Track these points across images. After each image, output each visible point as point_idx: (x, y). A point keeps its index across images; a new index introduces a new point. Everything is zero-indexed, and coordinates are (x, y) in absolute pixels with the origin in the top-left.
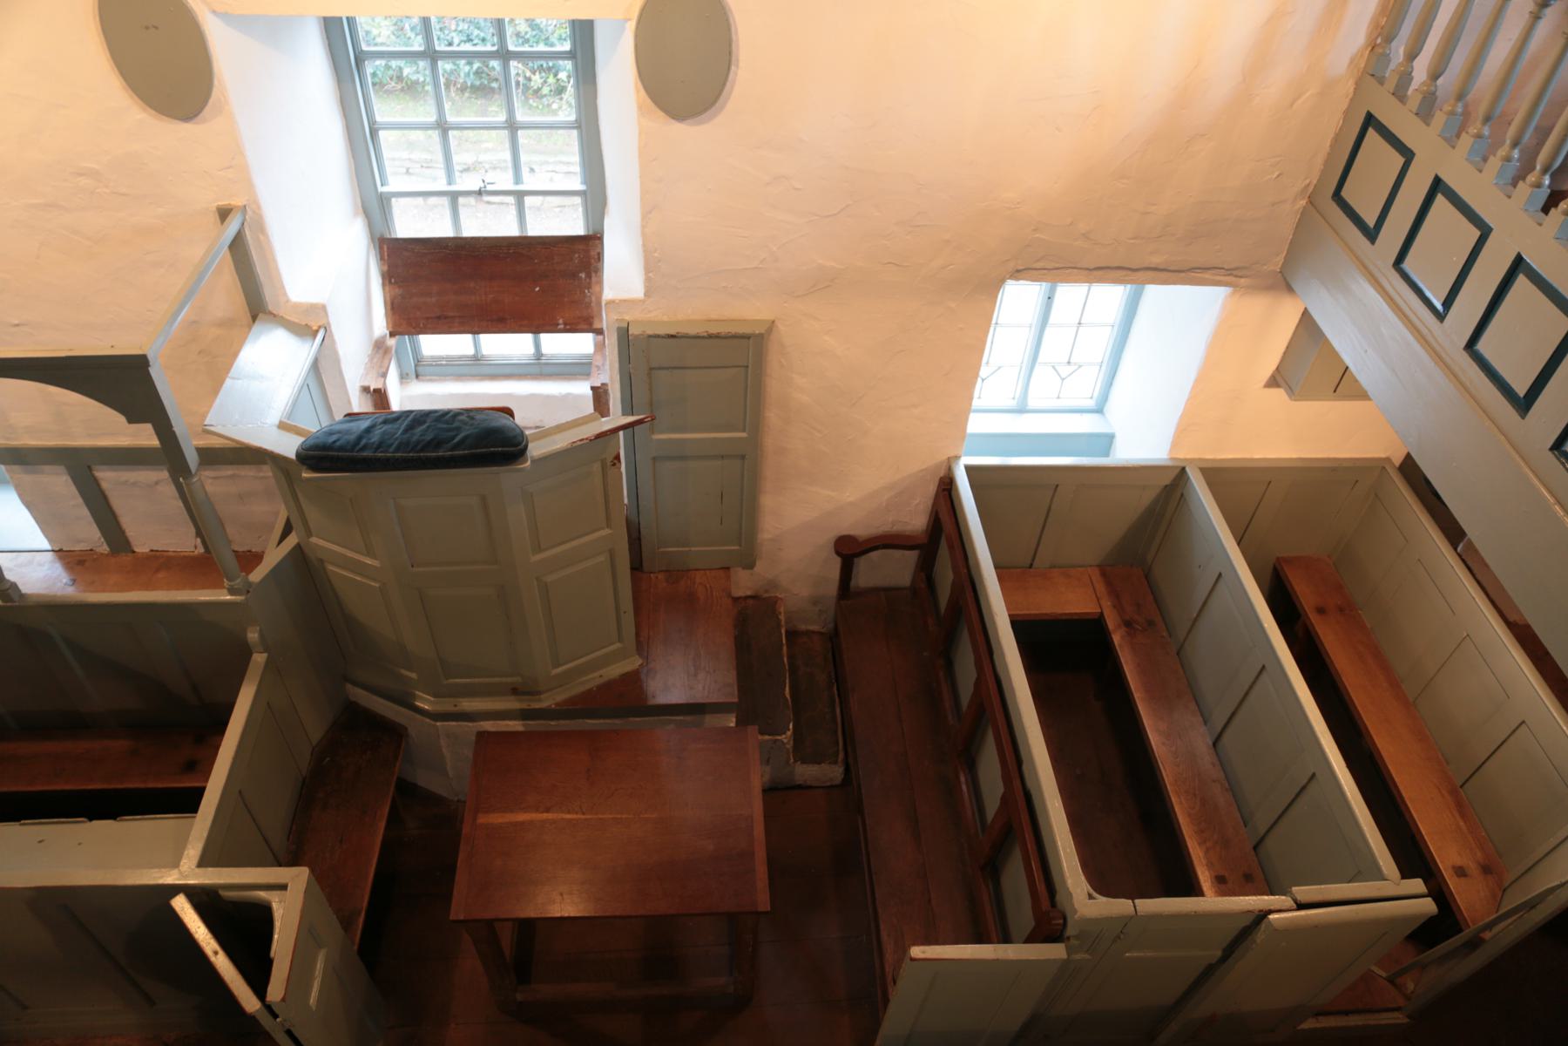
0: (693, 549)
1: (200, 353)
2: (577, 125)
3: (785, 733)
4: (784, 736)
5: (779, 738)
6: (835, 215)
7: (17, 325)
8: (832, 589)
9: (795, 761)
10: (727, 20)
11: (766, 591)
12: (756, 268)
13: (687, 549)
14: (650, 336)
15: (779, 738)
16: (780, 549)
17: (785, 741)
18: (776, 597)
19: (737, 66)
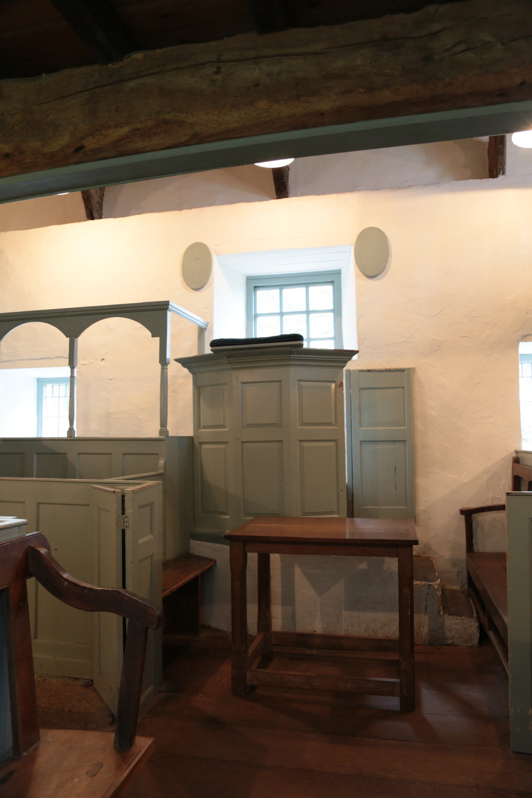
0: (381, 507)
1: (173, 391)
2: (333, 311)
3: (435, 581)
4: (435, 583)
5: (431, 583)
6: (436, 315)
7: (111, 379)
8: (462, 553)
9: (444, 614)
10: (388, 251)
11: (424, 553)
12: (405, 341)
13: (378, 507)
14: (360, 371)
15: (431, 583)
16: (429, 518)
17: (436, 587)
18: (430, 556)
19: (391, 257)
